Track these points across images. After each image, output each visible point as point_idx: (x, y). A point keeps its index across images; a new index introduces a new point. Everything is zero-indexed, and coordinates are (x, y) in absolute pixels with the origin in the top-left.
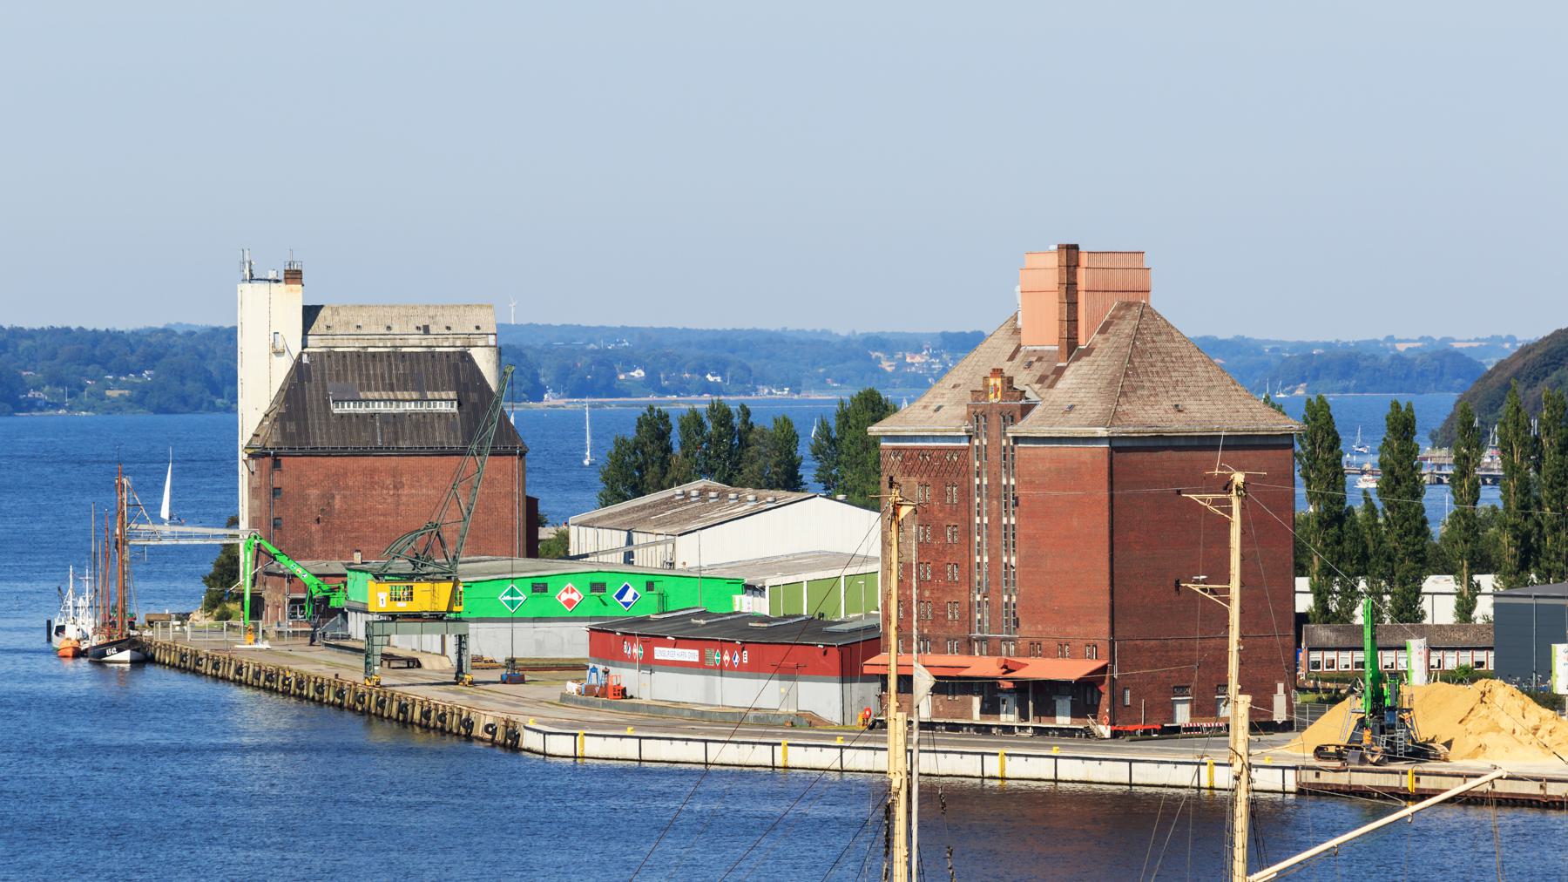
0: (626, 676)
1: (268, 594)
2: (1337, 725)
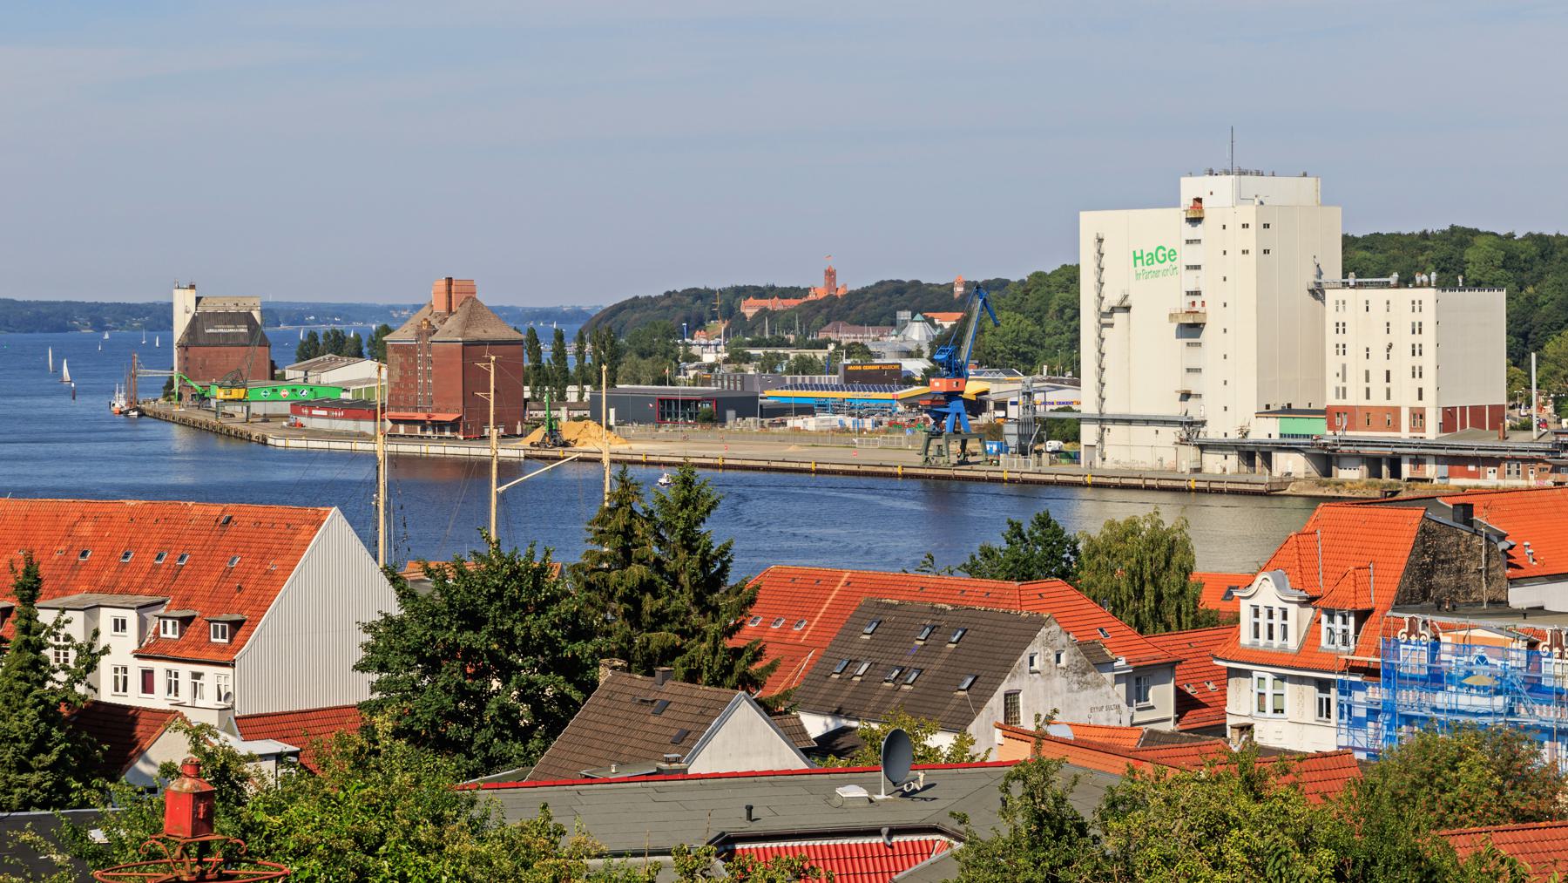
0: (302, 420)
1: (184, 393)
2: (538, 435)
